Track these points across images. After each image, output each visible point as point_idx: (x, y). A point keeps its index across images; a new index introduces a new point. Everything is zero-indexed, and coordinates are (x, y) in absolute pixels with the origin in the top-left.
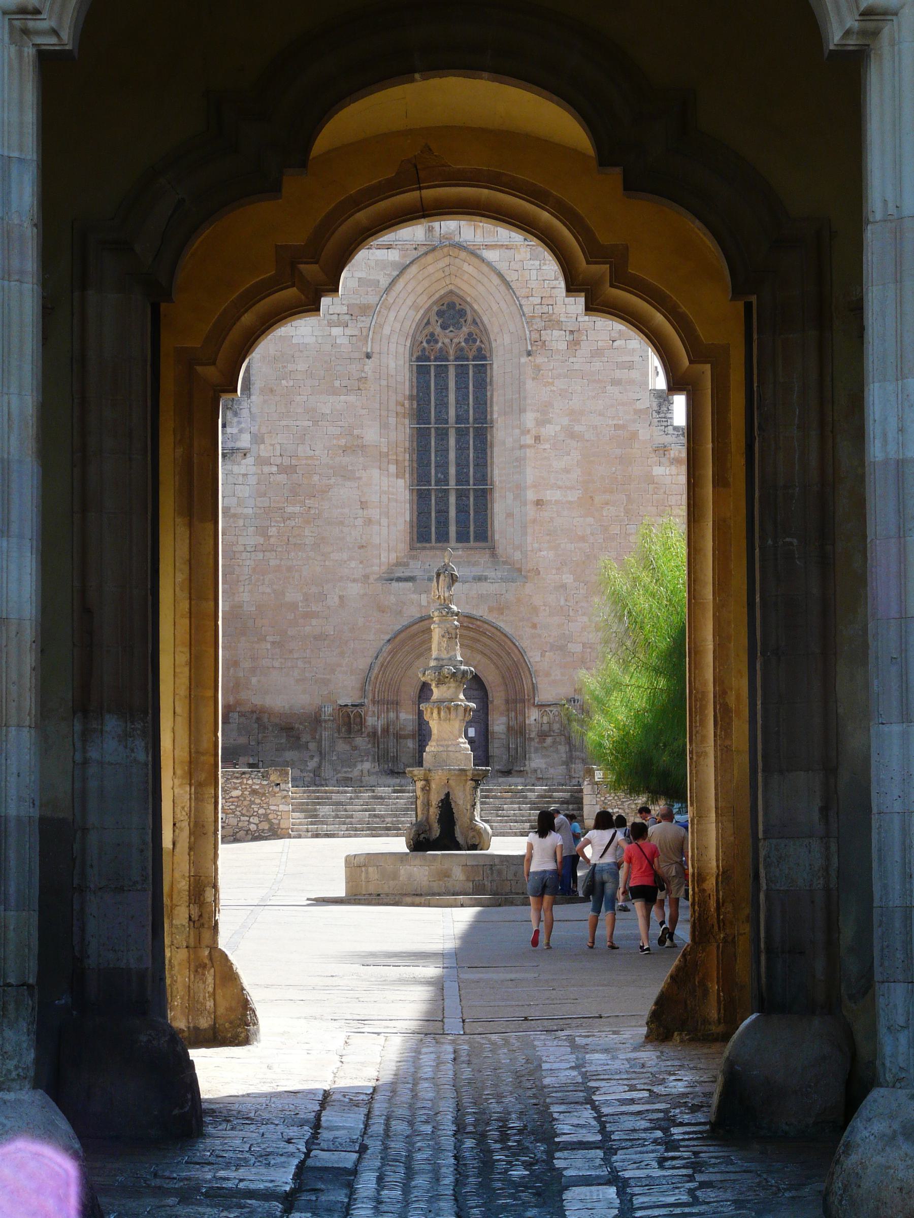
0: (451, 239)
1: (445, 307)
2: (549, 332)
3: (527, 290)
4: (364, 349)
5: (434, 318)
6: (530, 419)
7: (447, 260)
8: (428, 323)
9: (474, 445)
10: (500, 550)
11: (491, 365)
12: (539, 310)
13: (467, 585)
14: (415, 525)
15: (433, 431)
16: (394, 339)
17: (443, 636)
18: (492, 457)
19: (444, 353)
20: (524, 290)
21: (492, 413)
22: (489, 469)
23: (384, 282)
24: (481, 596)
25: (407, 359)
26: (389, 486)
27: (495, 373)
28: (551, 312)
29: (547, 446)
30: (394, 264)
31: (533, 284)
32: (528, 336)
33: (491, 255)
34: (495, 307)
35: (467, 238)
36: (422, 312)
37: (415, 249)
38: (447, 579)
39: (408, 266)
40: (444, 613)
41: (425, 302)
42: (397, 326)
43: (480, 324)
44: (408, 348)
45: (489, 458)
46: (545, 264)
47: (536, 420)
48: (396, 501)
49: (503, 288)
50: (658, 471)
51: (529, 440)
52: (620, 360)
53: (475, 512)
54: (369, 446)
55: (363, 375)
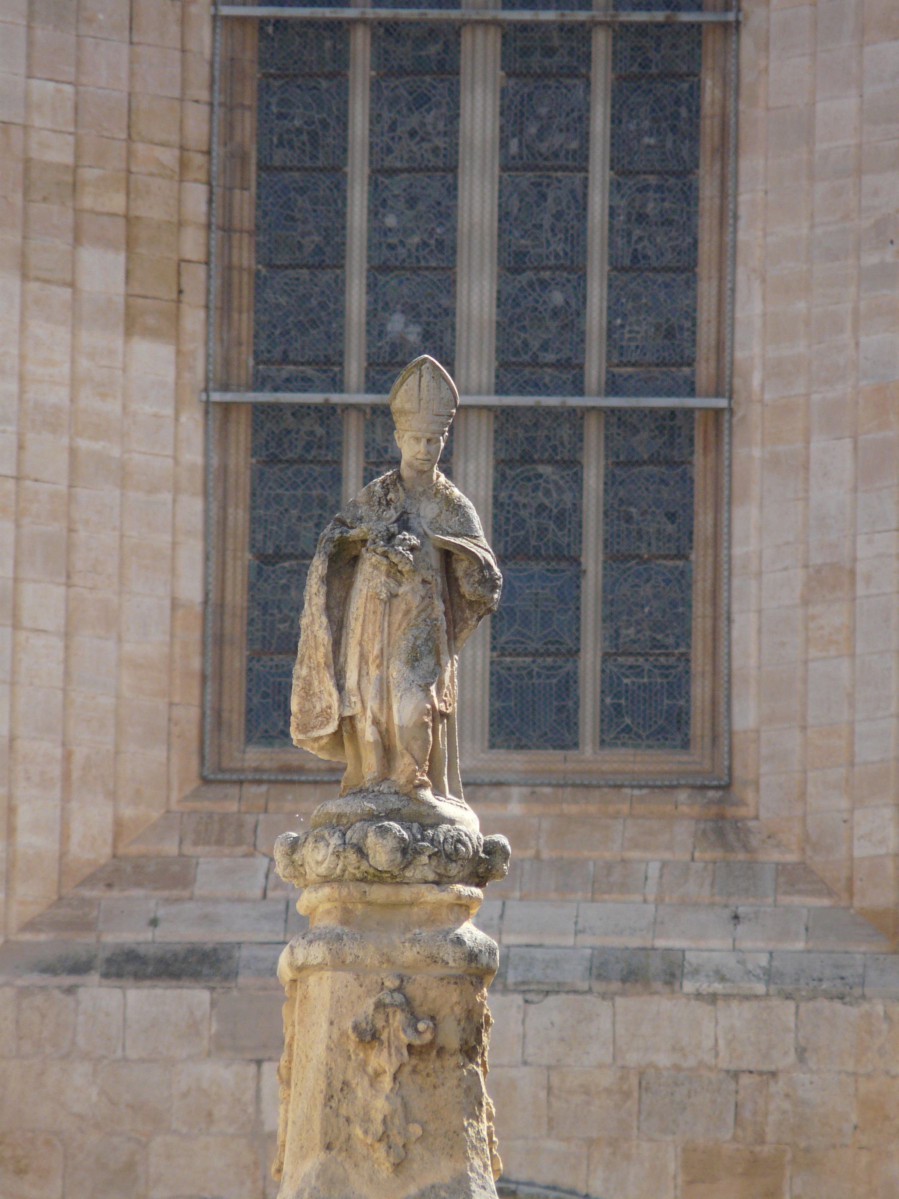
9: (618, 141)
10: (765, 799)
13: (552, 1011)
14: (236, 627)
15: (361, 45)
17: (369, 1036)
18: (727, 217)
22: (707, 289)
24: (639, 1087)
26: (75, 383)
40: (381, 854)
45: (707, 225)
48: (123, 476)
53: (616, 557)
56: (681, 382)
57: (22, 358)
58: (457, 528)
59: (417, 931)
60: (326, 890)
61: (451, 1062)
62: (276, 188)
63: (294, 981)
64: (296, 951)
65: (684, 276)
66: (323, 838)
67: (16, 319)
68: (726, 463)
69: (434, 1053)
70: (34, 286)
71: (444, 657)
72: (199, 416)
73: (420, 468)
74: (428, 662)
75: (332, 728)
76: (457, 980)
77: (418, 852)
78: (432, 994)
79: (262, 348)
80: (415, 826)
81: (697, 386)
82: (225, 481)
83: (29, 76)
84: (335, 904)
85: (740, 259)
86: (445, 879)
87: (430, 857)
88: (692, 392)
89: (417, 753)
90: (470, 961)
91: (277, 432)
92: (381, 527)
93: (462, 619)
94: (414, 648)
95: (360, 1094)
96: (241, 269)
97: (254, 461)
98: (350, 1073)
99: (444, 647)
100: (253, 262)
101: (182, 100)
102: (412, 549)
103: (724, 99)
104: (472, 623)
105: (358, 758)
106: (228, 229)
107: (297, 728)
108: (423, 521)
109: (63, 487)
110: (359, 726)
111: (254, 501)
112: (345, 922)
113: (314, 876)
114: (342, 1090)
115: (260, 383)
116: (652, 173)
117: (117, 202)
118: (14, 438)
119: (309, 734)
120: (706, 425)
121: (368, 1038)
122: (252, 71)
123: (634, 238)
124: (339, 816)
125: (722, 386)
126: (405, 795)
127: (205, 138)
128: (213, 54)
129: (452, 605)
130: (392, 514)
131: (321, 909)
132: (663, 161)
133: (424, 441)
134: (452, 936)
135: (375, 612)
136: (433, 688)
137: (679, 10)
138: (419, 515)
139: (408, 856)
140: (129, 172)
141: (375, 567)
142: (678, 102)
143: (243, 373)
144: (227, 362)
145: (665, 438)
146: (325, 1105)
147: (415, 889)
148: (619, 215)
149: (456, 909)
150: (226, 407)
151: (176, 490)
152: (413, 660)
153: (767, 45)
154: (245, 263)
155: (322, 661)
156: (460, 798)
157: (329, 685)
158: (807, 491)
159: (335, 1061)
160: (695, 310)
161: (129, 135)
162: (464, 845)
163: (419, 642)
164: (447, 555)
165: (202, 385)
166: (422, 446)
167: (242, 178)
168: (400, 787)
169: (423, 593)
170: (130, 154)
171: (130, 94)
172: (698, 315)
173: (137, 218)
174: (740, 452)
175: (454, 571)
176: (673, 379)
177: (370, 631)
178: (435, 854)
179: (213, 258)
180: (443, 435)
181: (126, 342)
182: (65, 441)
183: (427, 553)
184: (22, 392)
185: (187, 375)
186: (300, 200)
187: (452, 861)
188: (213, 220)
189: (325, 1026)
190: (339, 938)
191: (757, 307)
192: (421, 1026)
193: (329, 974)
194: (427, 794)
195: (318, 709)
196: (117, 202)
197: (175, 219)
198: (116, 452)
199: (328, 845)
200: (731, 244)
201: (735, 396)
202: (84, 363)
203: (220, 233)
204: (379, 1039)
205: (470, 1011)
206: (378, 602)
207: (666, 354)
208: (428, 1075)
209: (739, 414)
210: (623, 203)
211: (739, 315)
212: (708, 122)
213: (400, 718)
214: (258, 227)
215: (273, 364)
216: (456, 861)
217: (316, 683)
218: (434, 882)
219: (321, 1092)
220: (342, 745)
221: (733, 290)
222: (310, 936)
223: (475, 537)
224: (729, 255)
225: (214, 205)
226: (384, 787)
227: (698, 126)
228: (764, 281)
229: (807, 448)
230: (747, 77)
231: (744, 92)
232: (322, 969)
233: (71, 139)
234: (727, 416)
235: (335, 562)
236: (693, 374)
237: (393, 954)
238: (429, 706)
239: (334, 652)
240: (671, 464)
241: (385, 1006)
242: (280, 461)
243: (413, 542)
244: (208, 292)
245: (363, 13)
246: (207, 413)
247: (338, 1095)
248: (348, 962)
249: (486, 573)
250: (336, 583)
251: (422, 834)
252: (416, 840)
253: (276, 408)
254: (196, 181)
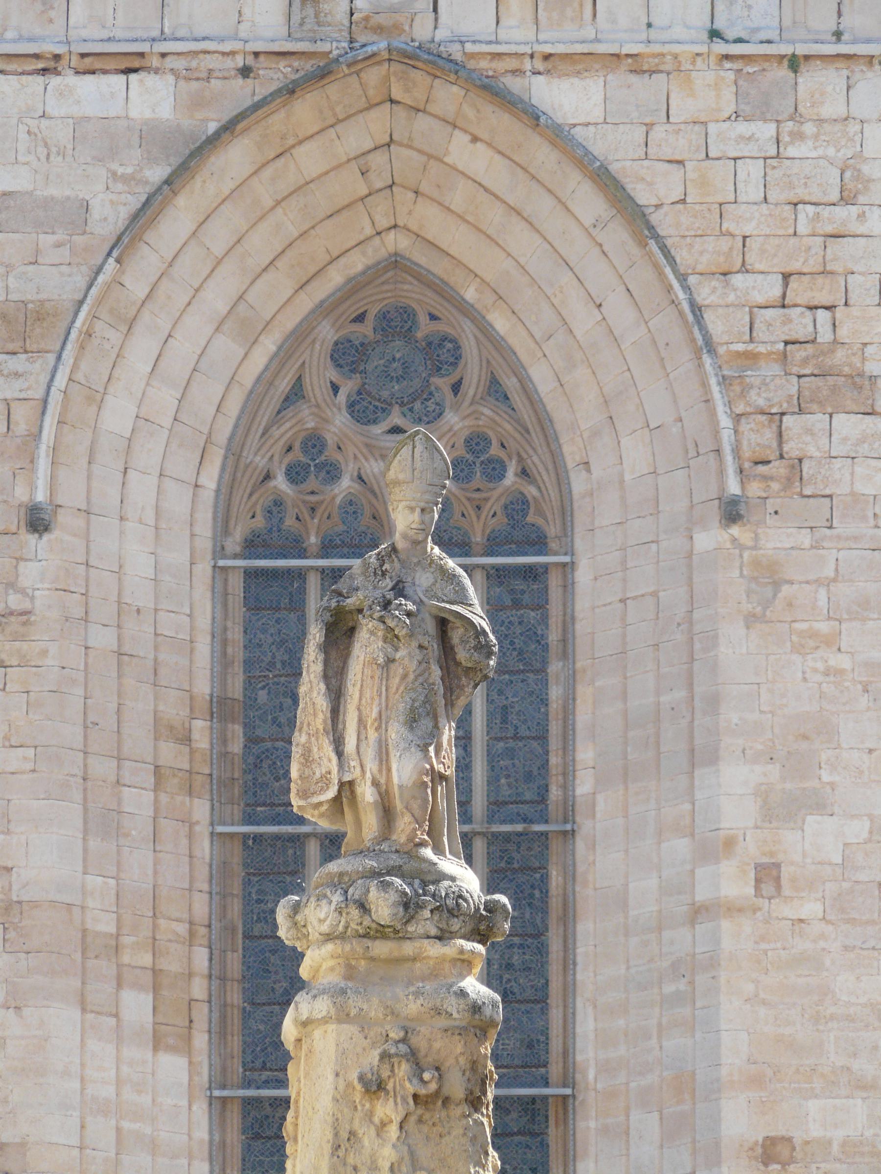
0: (397, 28)
1: (367, 330)
2: (818, 420)
3: (724, 244)
4: (21, 494)
5: (320, 373)
6: (734, 790)
7: (377, 124)
8: (296, 394)
11: (567, 569)
12: (773, 329)
16: (149, 453)
17: (375, 1087)
18: (568, 964)
19: (366, 520)
20: (710, 244)
21: (568, 773)
22: (555, 1014)
23: (110, 211)
25: (205, 544)
26: (119, 1082)
27: (582, 604)
28: (825, 335)
29: (811, 909)
30: (149, 135)
31: (749, 221)
32: (727, 436)
33: (568, 99)
34: (583, 321)
35: (467, 28)
36: (269, 345)
37: (245, 72)
38: (407, 656)
39: (213, 141)
40: (383, 907)
41: (282, 302)
42: (165, 398)
43: (517, 399)
44: (208, 495)
46: (798, 136)
47: (763, 794)
48: (154, 1147)
49: (617, 236)
51: (731, 882)
54: (35, 904)
55: (14, 601)
56: (539, 1078)
57: (83, 1065)
58: (452, 596)
59: (421, 985)
60: (330, 947)
61: (457, 1111)
62: (256, 950)
63: (299, 1040)
64: (299, 1006)
65: (540, 1006)
66: (325, 896)
67: (79, 1038)
68: (571, 1132)
69: (440, 1103)
70: (90, 1016)
71: (442, 721)
72: (205, 1106)
73: (415, 537)
74: (426, 723)
75: (331, 793)
76: (462, 1031)
77: (420, 907)
78: (437, 1045)
79: (248, 1060)
80: (417, 882)
81: (550, 1081)
82: (224, 1151)
83: (85, 873)
84: (340, 960)
85: (579, 992)
86: (447, 935)
87: (432, 911)
88: (547, 1084)
89: (417, 812)
90: (474, 1012)
91: (259, 1117)
92: (378, 594)
93: (458, 687)
94: (412, 710)
95: (366, 1143)
96: (232, 1006)
97: (244, 1137)
98: (356, 1123)
99: (441, 710)
100: (241, 1001)
101: (190, 890)
102: (409, 614)
103: (565, 883)
104: (468, 690)
105: (358, 823)
106: (223, 979)
107: (298, 794)
108: (418, 589)
109: (113, 1154)
110: (359, 790)
111: (244, 1165)
112: (348, 977)
113: (317, 935)
114: (349, 1139)
115: (247, 1084)
116: (517, 935)
117: (147, 959)
118: (78, 1120)
119: (309, 800)
120: (557, 1106)
121: (374, 1088)
122: (239, 871)
123: (504, 980)
124: (341, 875)
125: (568, 1080)
126: (406, 853)
127: (207, 916)
128: (211, 859)
129: (449, 673)
130: (388, 583)
131: (324, 967)
132: (524, 927)
133: (418, 510)
134: (455, 988)
135: (372, 677)
136: (432, 749)
137: (533, 823)
138: (414, 584)
139: (410, 910)
140: (154, 939)
141: (372, 633)
142: (533, 887)
143: (235, 1077)
144: (224, 1070)
145: (528, 1117)
146: (333, 1155)
147: (417, 944)
148: (494, 965)
149: (459, 964)
150: (224, 1100)
151: (190, 1157)
152: (412, 721)
153: (594, 846)
154: (235, 1002)
155: (321, 727)
156: (460, 858)
157: (329, 750)
158: (628, 1150)
159: (342, 1112)
160: (547, 1029)
161: (154, 914)
162: (466, 900)
163: (417, 704)
164: (443, 623)
165: (207, 1086)
166: (416, 516)
167: (232, 944)
168: (401, 845)
169: (420, 658)
170: (155, 927)
171: (154, 886)
172: (550, 1032)
173: (161, 970)
174: (581, 1125)
175: (450, 639)
176: (533, 1076)
177: (368, 696)
178: (437, 908)
179: (213, 999)
180: (437, 505)
181: (154, 1055)
182: (113, 1122)
183: (423, 620)
184: (83, 1089)
185: (196, 1078)
186: (272, 959)
187: (454, 916)
188: (213, 972)
189: (331, 1077)
190: (343, 992)
191: (591, 1025)
192: (427, 1076)
193: (334, 1026)
194: (428, 852)
195: (318, 775)
196: (147, 959)
197: (187, 972)
198: (148, 1130)
199: (330, 903)
200: (572, 982)
201: (576, 1087)
202: (125, 1069)
203: (218, 981)
204: (385, 1089)
205: (474, 1062)
206: (375, 667)
207: (528, 1059)
208: (434, 1124)
209: (580, 1098)
210: (497, 956)
211: (579, 1030)
212: (554, 900)
213: (400, 777)
214: (244, 977)
215: (256, 1070)
216: (457, 917)
217: (315, 750)
218: (436, 937)
219: (328, 1142)
220: (342, 812)
221: (574, 1014)
222: (314, 992)
223: (471, 605)
224: (570, 990)
225: (213, 962)
226: (385, 846)
227: (547, 902)
228: (595, 1007)
229: (628, 1120)
230: (581, 868)
231: (579, 879)
232: (327, 1022)
233: (115, 915)
234: (571, 1101)
235: (332, 632)
236: (547, 1072)
237: (397, 1006)
238: (428, 767)
239: (333, 721)
240: (533, 1134)
241: (390, 1056)
242: (262, 1137)
243: (409, 607)
244: (210, 1022)
245: (315, 829)
246: (210, 1104)
247: (344, 1145)
248: (352, 1014)
249: (482, 639)
250: (333, 654)
251: (424, 890)
252: (418, 895)
253: (259, 1100)
254: (201, 945)
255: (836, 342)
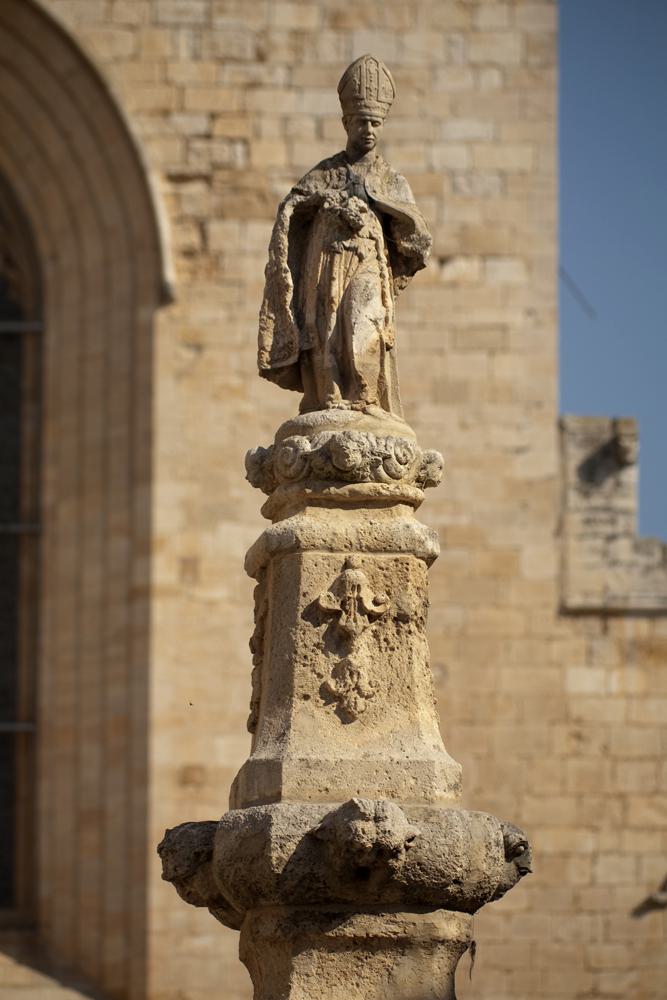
2: (232, 226)
18: (35, 632)
27: (51, 361)
28: (240, 162)
47: (186, 505)
50: (584, 681)
52: (463, 320)
110: (317, 358)
255: (249, 169)
